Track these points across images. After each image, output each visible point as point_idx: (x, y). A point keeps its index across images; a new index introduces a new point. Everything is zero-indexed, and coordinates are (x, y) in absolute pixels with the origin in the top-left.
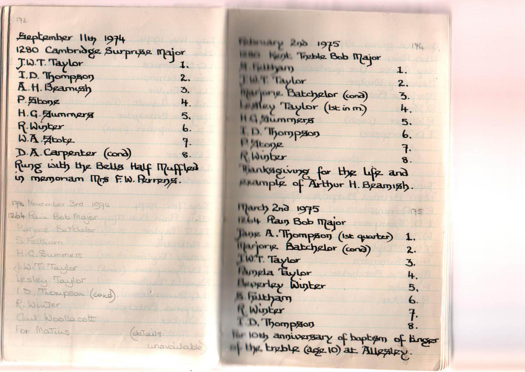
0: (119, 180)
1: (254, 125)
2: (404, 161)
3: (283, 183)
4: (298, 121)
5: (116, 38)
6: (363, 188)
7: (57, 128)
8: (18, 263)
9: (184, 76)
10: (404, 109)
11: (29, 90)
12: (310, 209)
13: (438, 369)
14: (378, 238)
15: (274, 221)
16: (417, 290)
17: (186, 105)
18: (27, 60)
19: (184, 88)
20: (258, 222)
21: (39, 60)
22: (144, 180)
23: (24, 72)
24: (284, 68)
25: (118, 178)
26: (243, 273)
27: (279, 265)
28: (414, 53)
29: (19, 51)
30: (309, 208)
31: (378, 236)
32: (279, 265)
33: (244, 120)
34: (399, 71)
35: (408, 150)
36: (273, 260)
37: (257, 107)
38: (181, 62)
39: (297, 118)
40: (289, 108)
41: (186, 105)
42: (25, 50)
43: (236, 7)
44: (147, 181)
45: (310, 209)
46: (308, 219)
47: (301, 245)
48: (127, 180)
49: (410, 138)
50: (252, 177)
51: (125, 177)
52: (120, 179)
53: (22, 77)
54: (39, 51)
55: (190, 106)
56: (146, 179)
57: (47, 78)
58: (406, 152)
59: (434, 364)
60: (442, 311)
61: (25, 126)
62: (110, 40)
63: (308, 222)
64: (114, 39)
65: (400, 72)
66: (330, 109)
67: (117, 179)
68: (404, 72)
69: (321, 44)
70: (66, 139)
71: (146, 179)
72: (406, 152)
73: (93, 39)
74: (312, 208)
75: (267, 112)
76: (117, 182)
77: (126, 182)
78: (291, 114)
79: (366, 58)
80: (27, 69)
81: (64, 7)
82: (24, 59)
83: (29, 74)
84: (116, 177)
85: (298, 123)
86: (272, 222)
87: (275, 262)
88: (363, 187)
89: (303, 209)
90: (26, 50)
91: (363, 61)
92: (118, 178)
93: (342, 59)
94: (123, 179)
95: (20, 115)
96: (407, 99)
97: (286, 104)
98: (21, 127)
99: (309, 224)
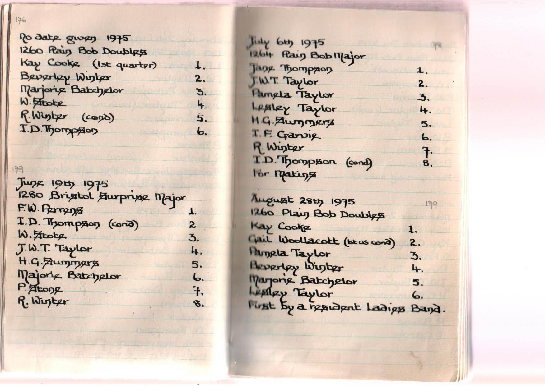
0: (21, 209)
1: (267, 127)
2: (424, 165)
3: (59, 289)
4: (317, 123)
5: (119, 37)
6: (341, 217)
7: (61, 117)
8: (131, 224)
9: (199, 76)
10: (423, 110)
11: (26, 224)
12: (346, 202)
13: (455, 381)
14: (141, 67)
15: (288, 55)
16: (428, 100)
17: (202, 108)
18: (28, 206)
19: (199, 90)
20: (270, 55)
21: (283, 65)
22: (50, 210)
23: (23, 218)
24: (262, 68)
25: (21, 206)
26: (256, 254)
27: (306, 259)
28: (431, 51)
29: (23, 51)
30: (345, 201)
31: (141, 64)
32: (306, 259)
33: (255, 122)
34: (419, 71)
35: (199, 293)
36: (298, 254)
37: (270, 109)
38: (418, 68)
39: (315, 119)
40: (307, 110)
41: (202, 108)
42: (28, 195)
43: (245, 5)
44: (53, 210)
45: (346, 202)
46: (92, 48)
47: (317, 278)
48: (30, 209)
49: (431, 140)
50: (293, 168)
51: (28, 206)
52: (23, 208)
53: (21, 223)
54: (44, 51)
55: (206, 108)
56: (52, 209)
57: (47, 131)
58: (197, 295)
59: (451, 375)
60: (459, 320)
61: (24, 301)
62: (114, 38)
63: (93, 51)
64: (117, 39)
65: (420, 72)
66: (99, 65)
67: (19, 208)
68: (425, 72)
69: (111, 37)
70: (57, 102)
71: (52, 209)
72: (197, 295)
73: (93, 39)
74: (348, 201)
75: (280, 114)
76: (19, 210)
77: (30, 211)
78: (311, 116)
79: (348, 57)
80: (28, 255)
81: (57, 5)
82: (24, 244)
83: (29, 220)
84: (19, 205)
85: (316, 125)
86: (54, 52)
87: (291, 83)
88: (341, 216)
89: (113, 37)
90: (29, 195)
91: (344, 60)
92: (21, 206)
93: (325, 57)
94: (26, 208)
95: (21, 263)
96: (427, 100)
97: (303, 105)
98: (257, 149)
99: (327, 58)
